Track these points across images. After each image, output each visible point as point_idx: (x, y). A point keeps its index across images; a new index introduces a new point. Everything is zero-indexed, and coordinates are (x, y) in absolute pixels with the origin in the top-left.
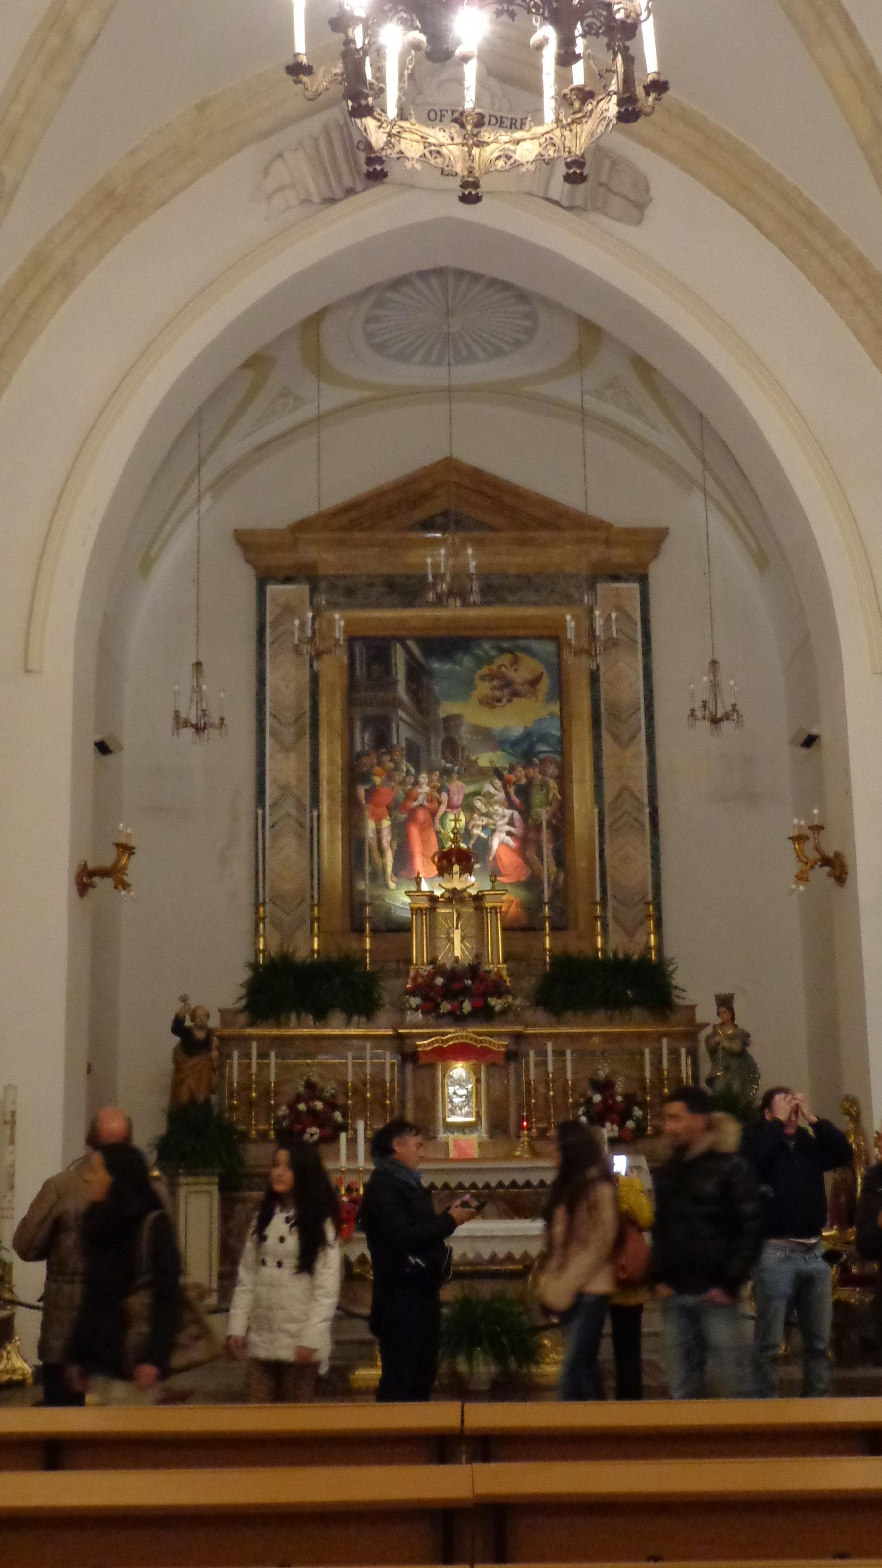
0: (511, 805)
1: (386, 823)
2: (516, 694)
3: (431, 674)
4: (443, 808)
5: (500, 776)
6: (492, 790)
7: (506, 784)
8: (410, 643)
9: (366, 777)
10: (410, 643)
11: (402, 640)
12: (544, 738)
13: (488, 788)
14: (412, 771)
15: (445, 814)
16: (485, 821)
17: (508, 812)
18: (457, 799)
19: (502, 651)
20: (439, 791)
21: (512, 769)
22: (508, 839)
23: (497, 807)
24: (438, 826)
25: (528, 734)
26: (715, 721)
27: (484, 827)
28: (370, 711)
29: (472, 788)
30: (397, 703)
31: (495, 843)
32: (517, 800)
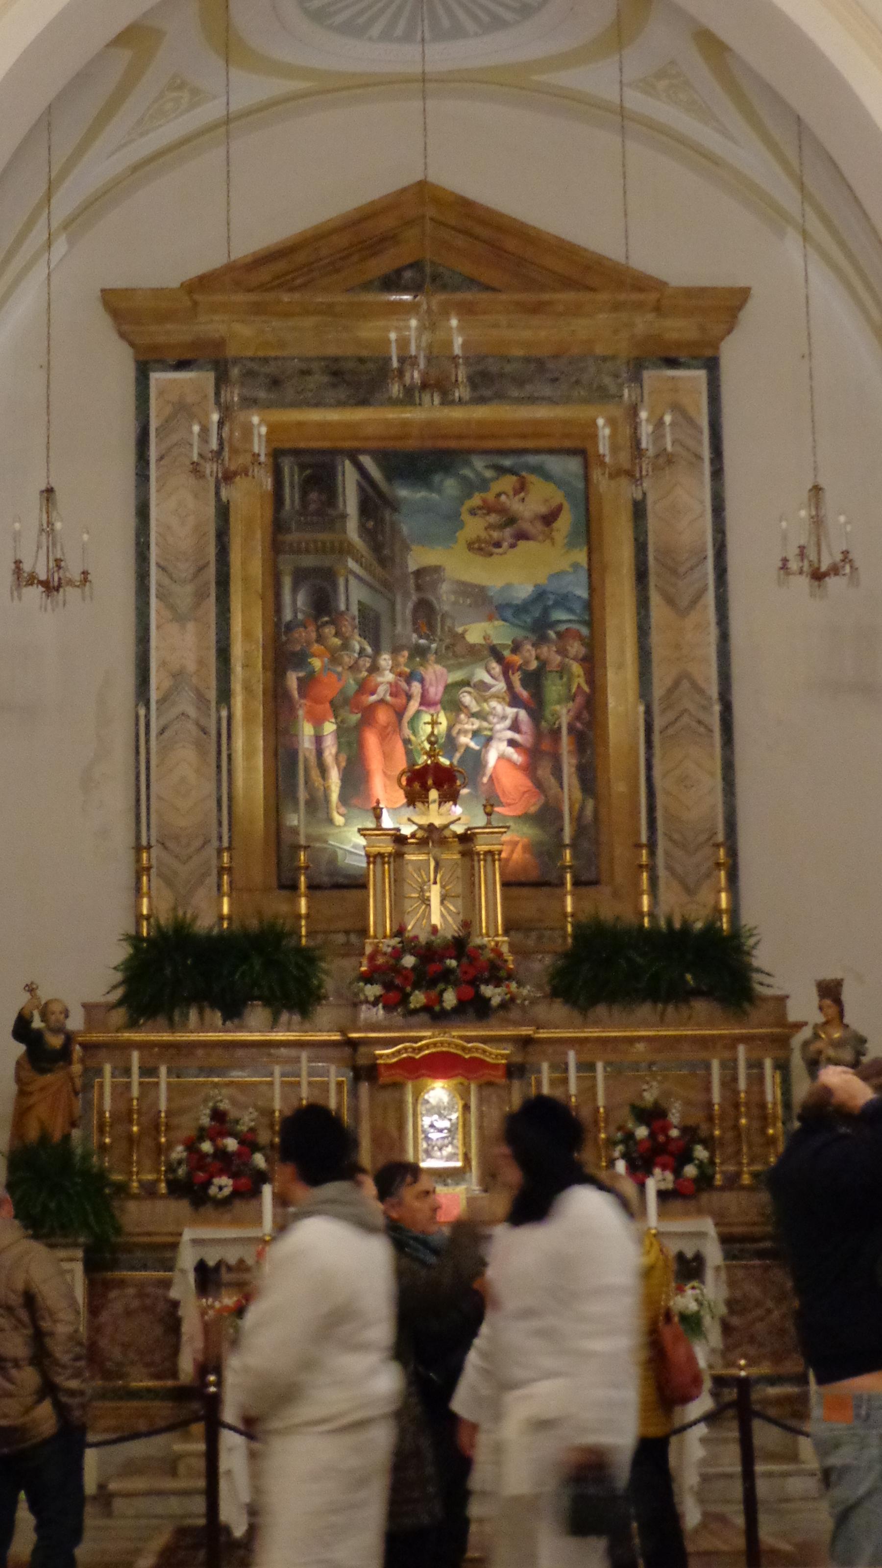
1: (329, 727)
2: (522, 536)
3: (394, 505)
4: (414, 705)
5: (500, 659)
6: (487, 679)
7: (507, 669)
8: (367, 461)
9: (300, 660)
10: (367, 461)
11: (353, 455)
12: (563, 601)
13: (481, 675)
14: (369, 650)
15: (418, 713)
17: (511, 711)
18: (436, 692)
19: (502, 471)
20: (409, 678)
21: (516, 648)
22: (510, 751)
23: (494, 703)
25: (540, 595)
26: (818, 576)
28: (309, 561)
30: (345, 549)
31: (492, 757)
32: (524, 694)
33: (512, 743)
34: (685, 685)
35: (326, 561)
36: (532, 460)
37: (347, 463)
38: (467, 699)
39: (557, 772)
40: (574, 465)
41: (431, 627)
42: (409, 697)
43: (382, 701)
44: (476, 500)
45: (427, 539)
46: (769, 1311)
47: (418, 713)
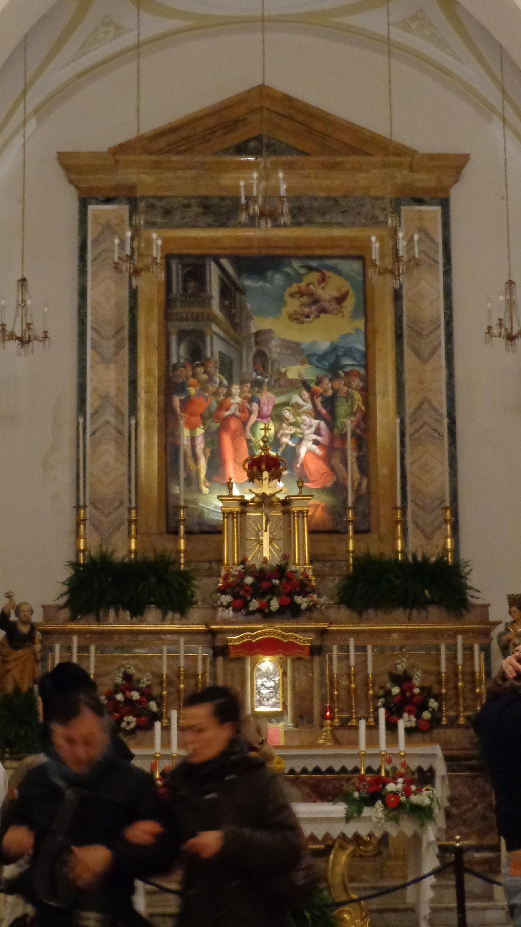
0: (317, 415)
1: (200, 431)
2: (323, 311)
3: (242, 291)
4: (254, 418)
6: (300, 401)
7: (313, 395)
8: (224, 262)
9: (181, 388)
10: (224, 262)
11: (216, 259)
12: (349, 352)
13: (296, 399)
14: (225, 382)
16: (293, 430)
17: (315, 422)
18: (267, 409)
19: (310, 269)
20: (251, 401)
21: (319, 382)
23: (304, 417)
24: (249, 435)
25: (334, 349)
27: (293, 436)
28: (188, 326)
29: (282, 399)
30: (211, 318)
31: (303, 451)
32: (324, 411)
33: (315, 442)
34: (426, 406)
35: (197, 326)
36: (330, 262)
37: (213, 263)
38: (287, 414)
39: (344, 461)
40: (356, 266)
41: (265, 368)
42: (251, 413)
43: (233, 415)
44: (294, 288)
45: (263, 313)
46: (476, 805)
47: (256, 423)
